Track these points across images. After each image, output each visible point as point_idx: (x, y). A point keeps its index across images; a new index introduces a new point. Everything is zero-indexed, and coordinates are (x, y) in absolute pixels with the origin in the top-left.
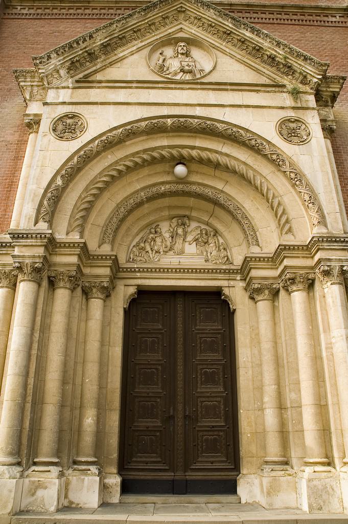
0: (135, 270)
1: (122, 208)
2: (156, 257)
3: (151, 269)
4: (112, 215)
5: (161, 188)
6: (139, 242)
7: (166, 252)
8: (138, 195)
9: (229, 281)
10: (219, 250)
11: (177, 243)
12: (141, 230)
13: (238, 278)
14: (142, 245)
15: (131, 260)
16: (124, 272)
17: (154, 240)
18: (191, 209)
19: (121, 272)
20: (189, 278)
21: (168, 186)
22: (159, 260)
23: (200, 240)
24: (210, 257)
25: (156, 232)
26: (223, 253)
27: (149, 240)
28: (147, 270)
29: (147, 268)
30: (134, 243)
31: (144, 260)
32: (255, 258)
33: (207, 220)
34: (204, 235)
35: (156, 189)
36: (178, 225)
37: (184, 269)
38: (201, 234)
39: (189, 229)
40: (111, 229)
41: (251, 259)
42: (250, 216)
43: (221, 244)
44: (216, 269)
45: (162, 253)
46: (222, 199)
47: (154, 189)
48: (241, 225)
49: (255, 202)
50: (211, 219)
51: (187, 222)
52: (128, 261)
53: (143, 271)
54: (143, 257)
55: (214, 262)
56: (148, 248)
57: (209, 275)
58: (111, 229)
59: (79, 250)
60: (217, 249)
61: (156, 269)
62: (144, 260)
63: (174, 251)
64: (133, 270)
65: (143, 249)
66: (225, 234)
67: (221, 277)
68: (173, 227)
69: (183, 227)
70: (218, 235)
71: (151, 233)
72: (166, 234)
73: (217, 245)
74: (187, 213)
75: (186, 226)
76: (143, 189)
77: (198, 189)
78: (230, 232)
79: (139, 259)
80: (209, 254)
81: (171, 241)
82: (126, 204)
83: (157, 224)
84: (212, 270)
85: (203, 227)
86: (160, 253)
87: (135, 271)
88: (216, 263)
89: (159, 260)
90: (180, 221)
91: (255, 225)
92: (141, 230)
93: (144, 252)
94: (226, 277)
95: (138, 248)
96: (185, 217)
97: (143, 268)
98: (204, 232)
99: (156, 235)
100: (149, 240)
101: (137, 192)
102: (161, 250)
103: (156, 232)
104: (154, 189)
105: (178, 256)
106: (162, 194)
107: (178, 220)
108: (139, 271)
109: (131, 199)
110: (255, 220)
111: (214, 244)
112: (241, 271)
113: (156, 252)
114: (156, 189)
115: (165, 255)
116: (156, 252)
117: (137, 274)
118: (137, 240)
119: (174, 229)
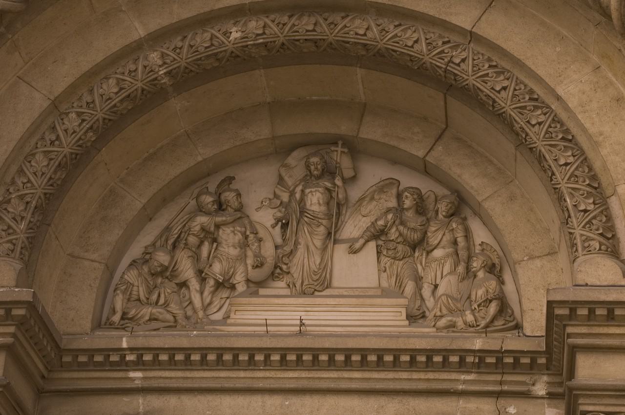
0: (123, 357)
1: (73, 115)
2: (217, 303)
3: (188, 351)
4: (33, 142)
5: (227, 34)
6: (154, 244)
7: (261, 284)
8: (136, 61)
9: (502, 402)
10: (469, 274)
11: (301, 249)
12: (164, 199)
13: (540, 389)
14: (162, 258)
15: (116, 318)
16: (82, 367)
17: (211, 236)
18: (363, 110)
19: (68, 367)
20: (332, 385)
21: (254, 25)
22: (227, 317)
23: (393, 234)
24: (430, 302)
25: (221, 207)
26: (484, 286)
27: (192, 240)
28: (171, 358)
29: (172, 351)
30: (136, 251)
31: (169, 317)
32: (591, 306)
33: (421, 154)
34: (410, 214)
35: (113, 82)
36: (309, 179)
37: (316, 352)
38: (400, 209)
39: (355, 193)
40: (21, 197)
41: (573, 310)
42: (584, 130)
43: (478, 249)
44: (446, 353)
45: (241, 288)
46: (468, 67)
47: (202, 39)
48: (545, 171)
49: (610, 75)
50: (439, 148)
51: (346, 163)
52: (99, 324)
53: (156, 364)
54: (166, 305)
55: (442, 322)
56: (187, 270)
57: (415, 376)
58: (21, 197)
59: (12, 329)
60: (461, 269)
61: (204, 351)
62: (169, 317)
63: (287, 279)
64: (114, 358)
65: (167, 273)
66: (495, 208)
67: (465, 382)
68: (290, 182)
69: (329, 185)
70: (467, 212)
71: (200, 210)
72: (261, 213)
73: (463, 254)
74: (345, 128)
75: (338, 182)
76: (157, 38)
77: (375, 32)
78: (512, 198)
79: (146, 312)
80: (426, 292)
81: (279, 241)
82: (87, 98)
83: (229, 172)
84: (430, 353)
85: (408, 180)
86: (233, 287)
87: (123, 365)
88: (452, 326)
89: (227, 317)
90: (314, 160)
91: (605, 168)
92: (164, 199)
93: (168, 288)
94: (487, 382)
95: (145, 269)
96: (335, 144)
97: (156, 351)
98: (408, 203)
99: (219, 219)
100: (192, 240)
101: (134, 49)
102: (239, 278)
103: (221, 207)
104: (202, 39)
105: (301, 300)
106: (234, 56)
107: (308, 157)
108: (139, 364)
109: (107, 78)
110: (604, 152)
111: (450, 250)
112: (549, 360)
113: (219, 285)
114: (207, 36)
115: (255, 294)
116: (219, 285)
117: (132, 374)
118: (147, 237)
119: (292, 194)
